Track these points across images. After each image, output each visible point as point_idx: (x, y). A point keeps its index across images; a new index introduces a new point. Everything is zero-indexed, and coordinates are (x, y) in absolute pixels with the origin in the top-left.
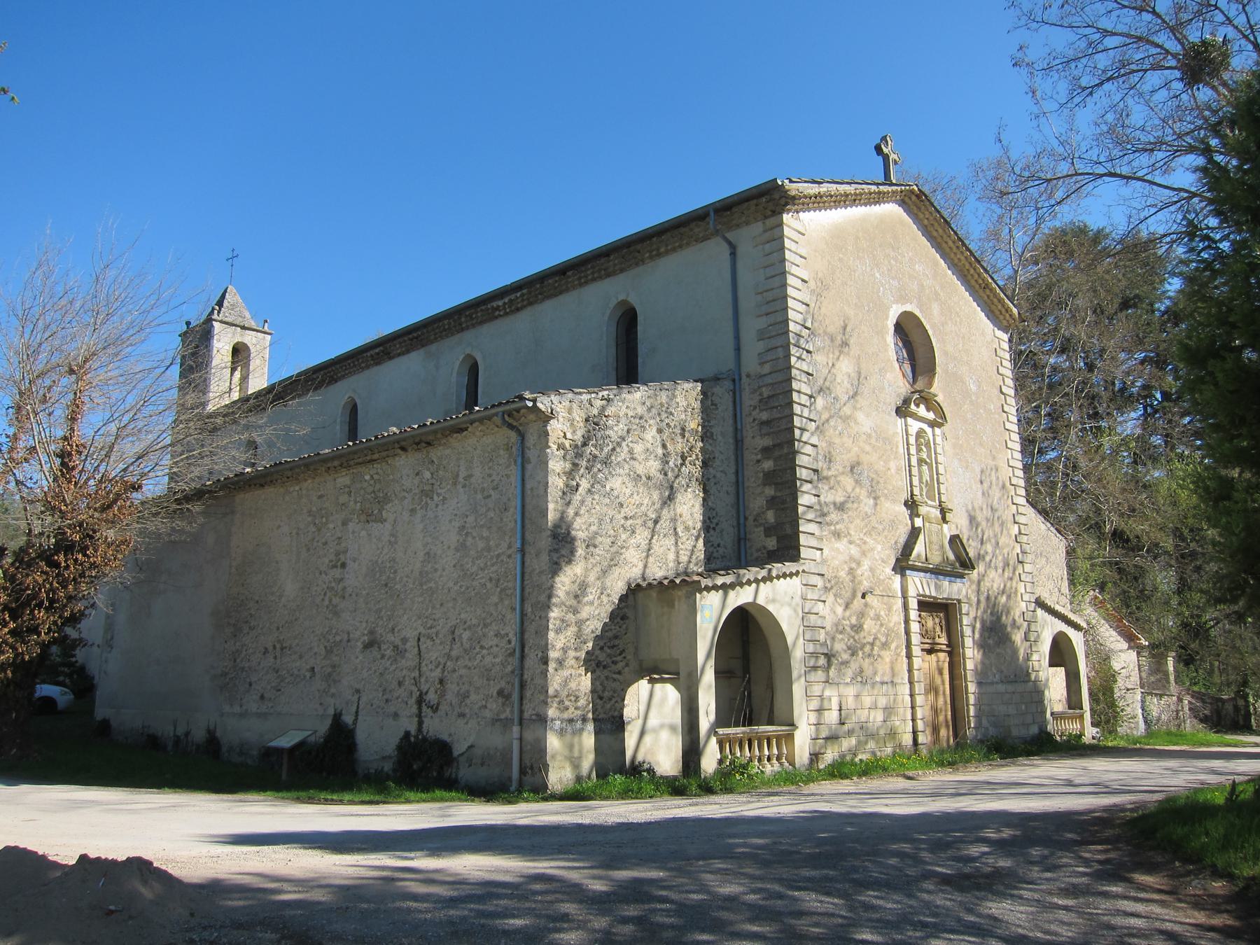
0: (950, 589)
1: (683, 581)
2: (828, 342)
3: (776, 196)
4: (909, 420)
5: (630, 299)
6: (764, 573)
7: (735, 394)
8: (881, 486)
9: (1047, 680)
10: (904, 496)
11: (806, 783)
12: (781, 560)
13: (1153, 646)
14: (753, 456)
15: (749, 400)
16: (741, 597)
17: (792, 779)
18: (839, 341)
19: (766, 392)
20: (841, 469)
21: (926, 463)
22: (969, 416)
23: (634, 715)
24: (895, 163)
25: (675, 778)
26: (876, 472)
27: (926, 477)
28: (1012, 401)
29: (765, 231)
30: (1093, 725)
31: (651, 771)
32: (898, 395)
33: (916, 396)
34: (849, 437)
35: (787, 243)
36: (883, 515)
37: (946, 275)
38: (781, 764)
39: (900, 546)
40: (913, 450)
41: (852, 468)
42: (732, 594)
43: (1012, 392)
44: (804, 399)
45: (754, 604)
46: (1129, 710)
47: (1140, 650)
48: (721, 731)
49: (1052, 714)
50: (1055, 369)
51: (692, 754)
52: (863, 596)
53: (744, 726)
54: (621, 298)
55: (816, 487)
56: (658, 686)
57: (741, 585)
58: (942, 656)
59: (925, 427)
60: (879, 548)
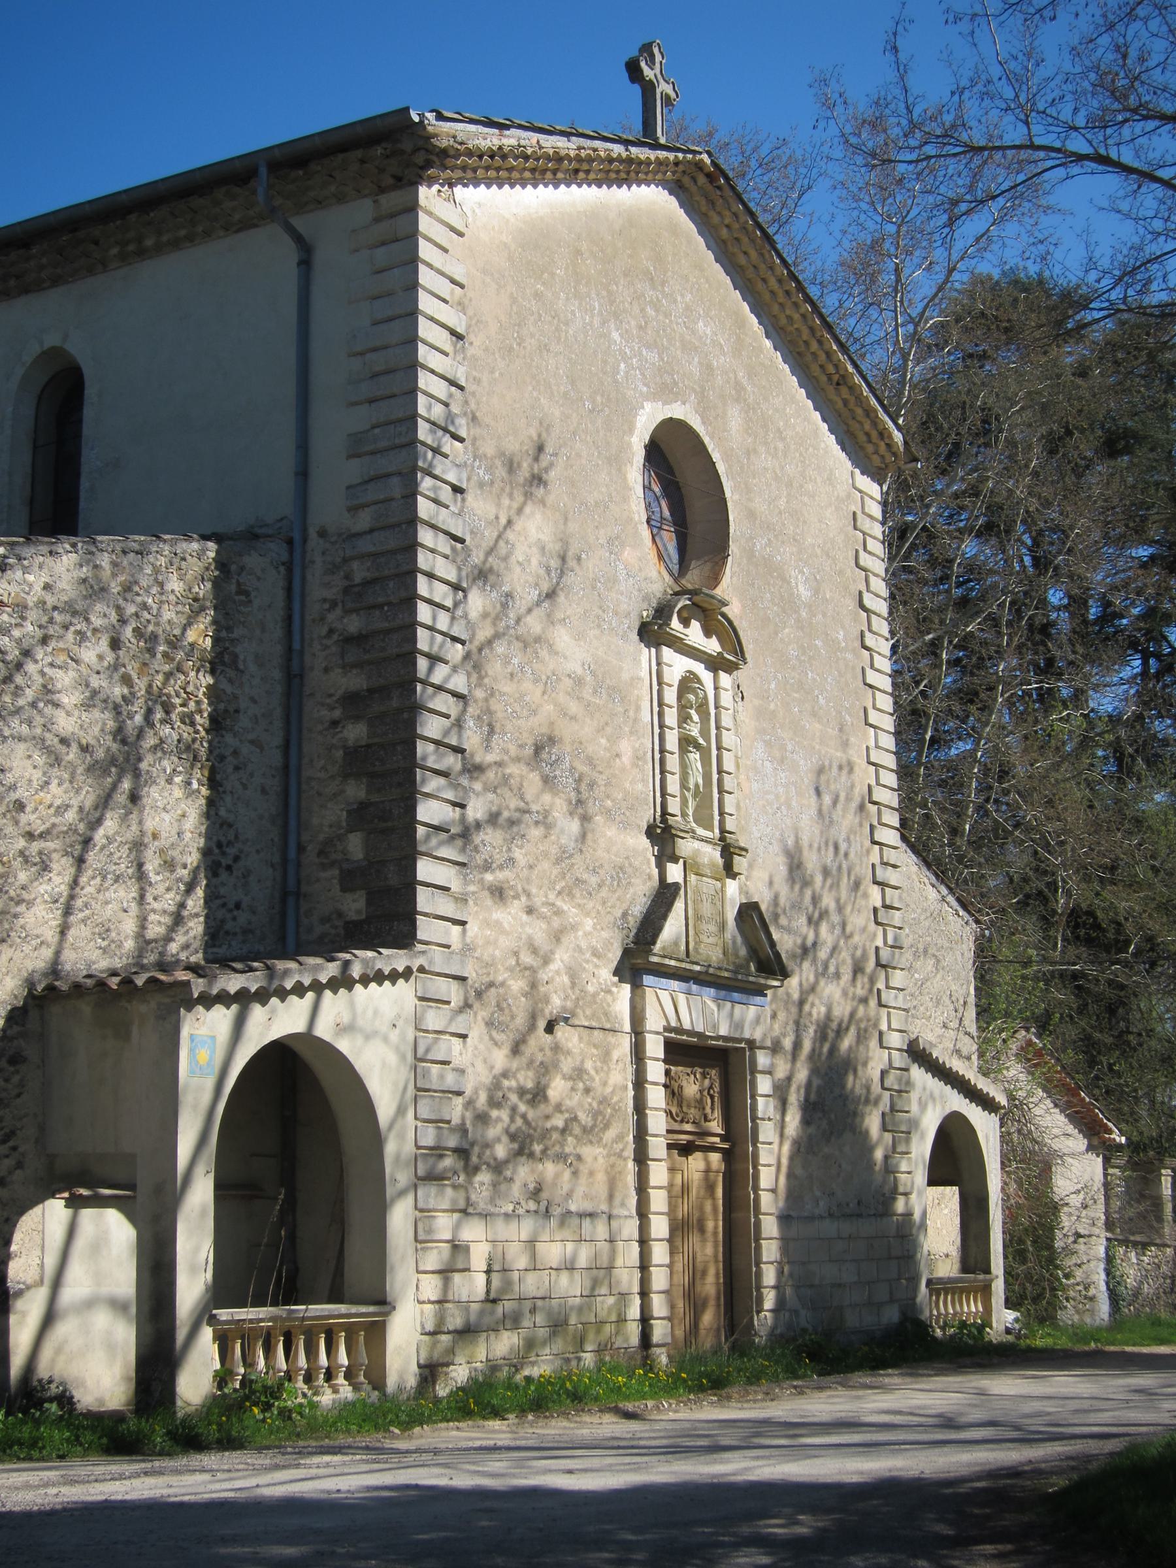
0: (751, 1019)
1: (152, 981)
2: (501, 472)
3: (407, 145)
4: (665, 650)
5: (69, 347)
6: (330, 970)
7: (292, 572)
8: (599, 792)
9: (924, 1214)
10: (646, 815)
11: (407, 1426)
12: (372, 943)
13: (1134, 1147)
14: (324, 712)
15: (320, 588)
16: (278, 1021)
17: (381, 1415)
18: (524, 472)
19: (359, 572)
20: (513, 750)
21: (697, 746)
22: (793, 651)
23: (30, 1276)
24: (667, 101)
25: (117, 1417)
26: (590, 761)
27: (696, 777)
28: (883, 627)
29: (377, 220)
30: (1009, 1304)
31: (65, 1400)
32: (646, 598)
33: (684, 602)
34: (536, 681)
35: (425, 250)
36: (600, 853)
37: (760, 349)
38: (356, 1387)
39: (633, 922)
40: (671, 718)
41: (538, 749)
42: (257, 1013)
43: (882, 607)
44: (440, 592)
45: (307, 1037)
46: (1079, 1274)
47: (1107, 1151)
48: (224, 1314)
49: (929, 1282)
50: (973, 569)
51: (157, 1361)
52: (550, 1028)
53: (275, 1304)
54: (52, 340)
55: (456, 787)
56: (87, 1214)
57: (283, 994)
58: (715, 1157)
59: (699, 668)
60: (588, 924)
